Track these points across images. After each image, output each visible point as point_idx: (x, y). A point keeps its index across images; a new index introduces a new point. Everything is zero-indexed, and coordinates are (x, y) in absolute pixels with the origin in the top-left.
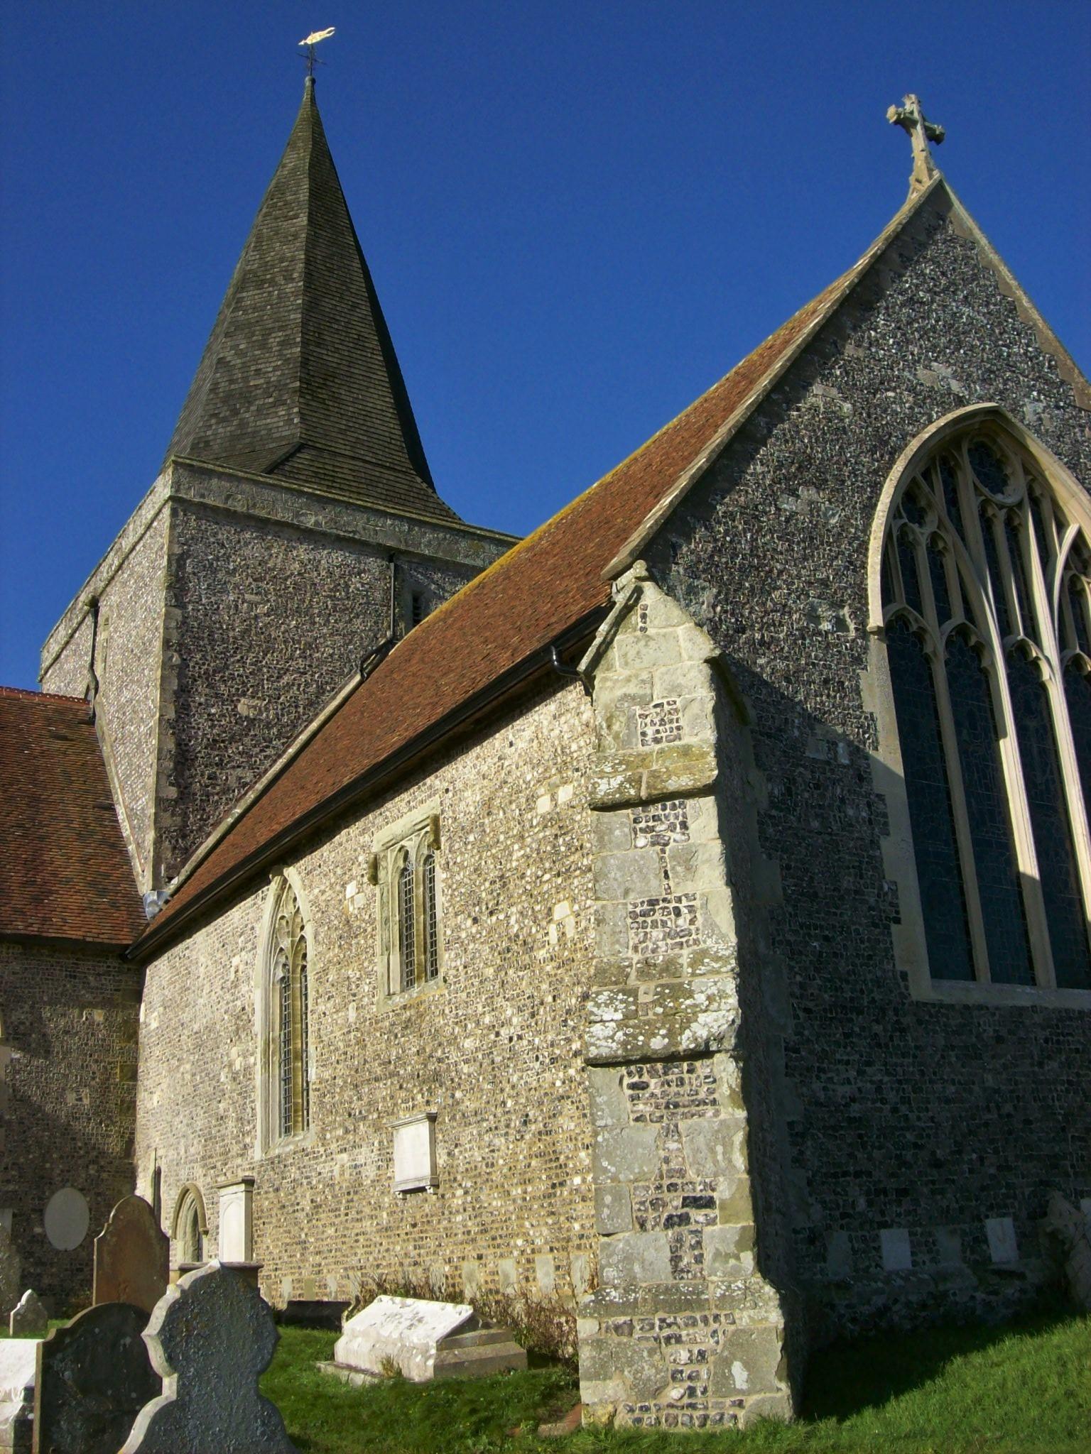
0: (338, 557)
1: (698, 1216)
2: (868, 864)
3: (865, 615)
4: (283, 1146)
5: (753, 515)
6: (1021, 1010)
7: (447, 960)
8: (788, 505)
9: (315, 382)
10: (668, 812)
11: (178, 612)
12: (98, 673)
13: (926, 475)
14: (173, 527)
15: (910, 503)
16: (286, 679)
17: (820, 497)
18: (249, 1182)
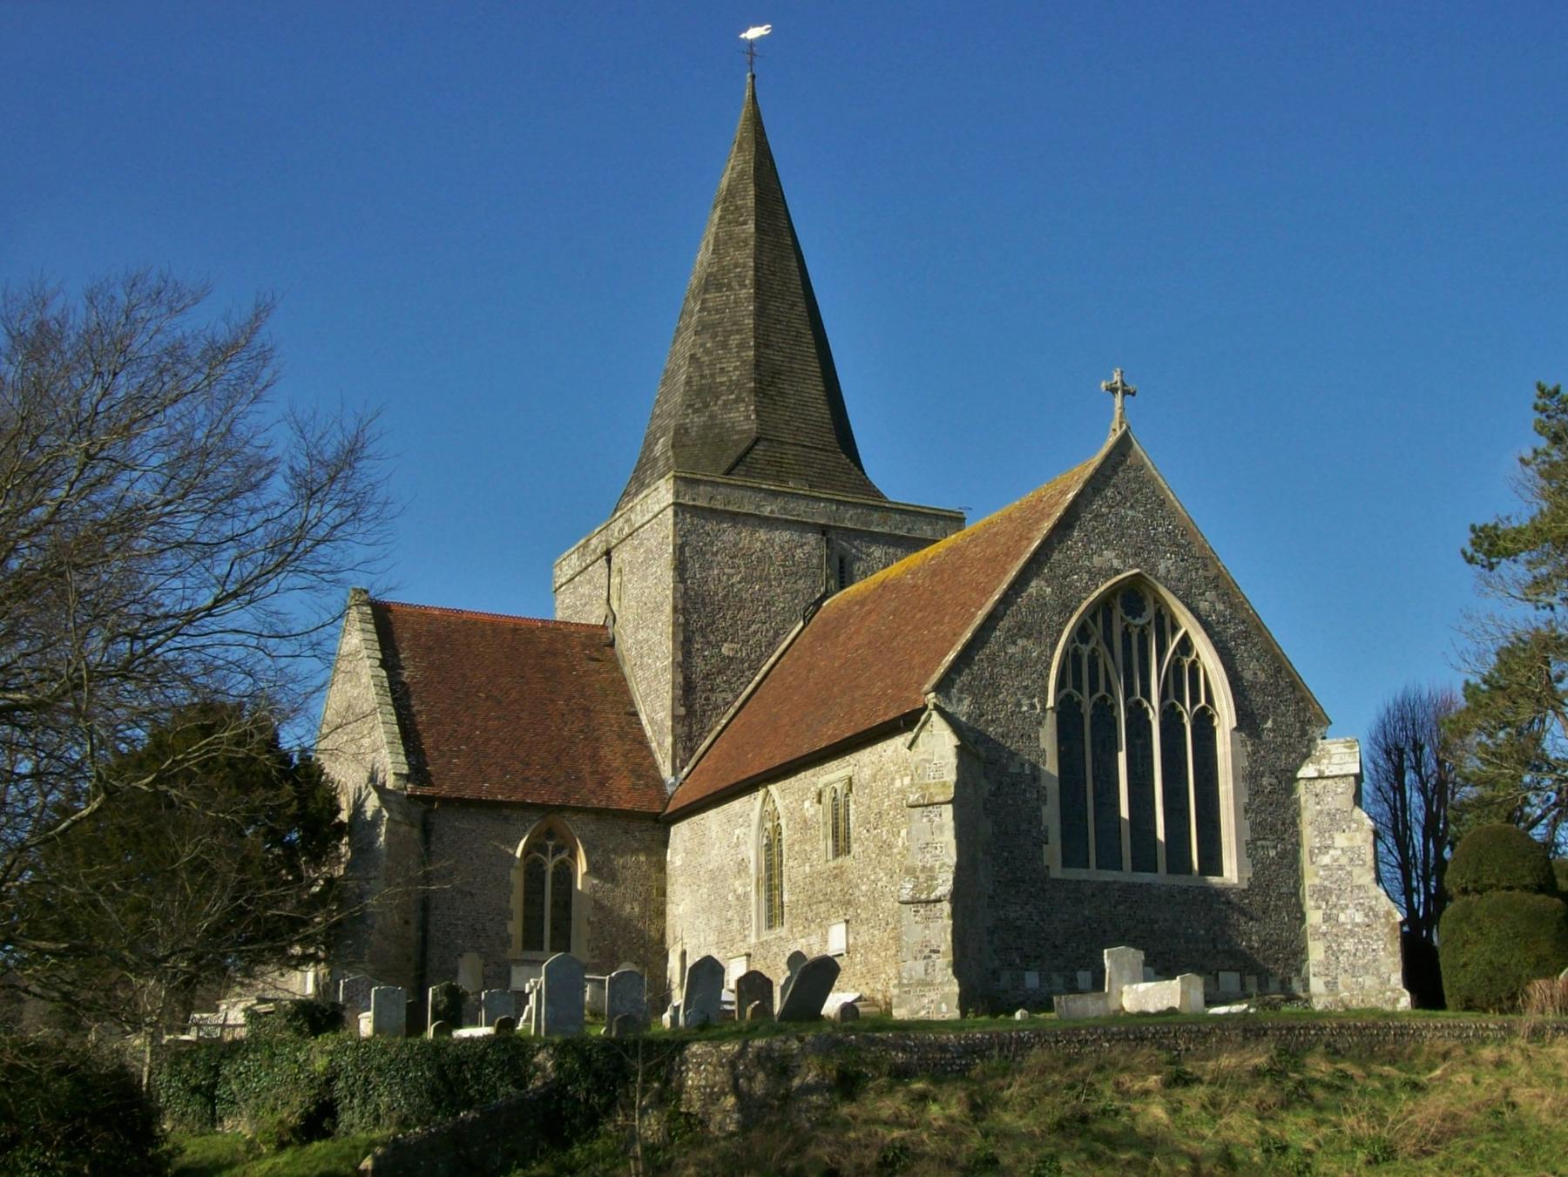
0: (786, 535)
1: (934, 956)
2: (1035, 817)
3: (1046, 700)
4: (767, 936)
5: (992, 659)
6: (1107, 883)
7: (855, 848)
8: (1011, 650)
9: (767, 381)
10: (935, 810)
11: (681, 586)
12: (615, 607)
13: (1093, 617)
14: (675, 524)
15: (1082, 633)
16: (754, 627)
17: (1029, 644)
18: (748, 955)
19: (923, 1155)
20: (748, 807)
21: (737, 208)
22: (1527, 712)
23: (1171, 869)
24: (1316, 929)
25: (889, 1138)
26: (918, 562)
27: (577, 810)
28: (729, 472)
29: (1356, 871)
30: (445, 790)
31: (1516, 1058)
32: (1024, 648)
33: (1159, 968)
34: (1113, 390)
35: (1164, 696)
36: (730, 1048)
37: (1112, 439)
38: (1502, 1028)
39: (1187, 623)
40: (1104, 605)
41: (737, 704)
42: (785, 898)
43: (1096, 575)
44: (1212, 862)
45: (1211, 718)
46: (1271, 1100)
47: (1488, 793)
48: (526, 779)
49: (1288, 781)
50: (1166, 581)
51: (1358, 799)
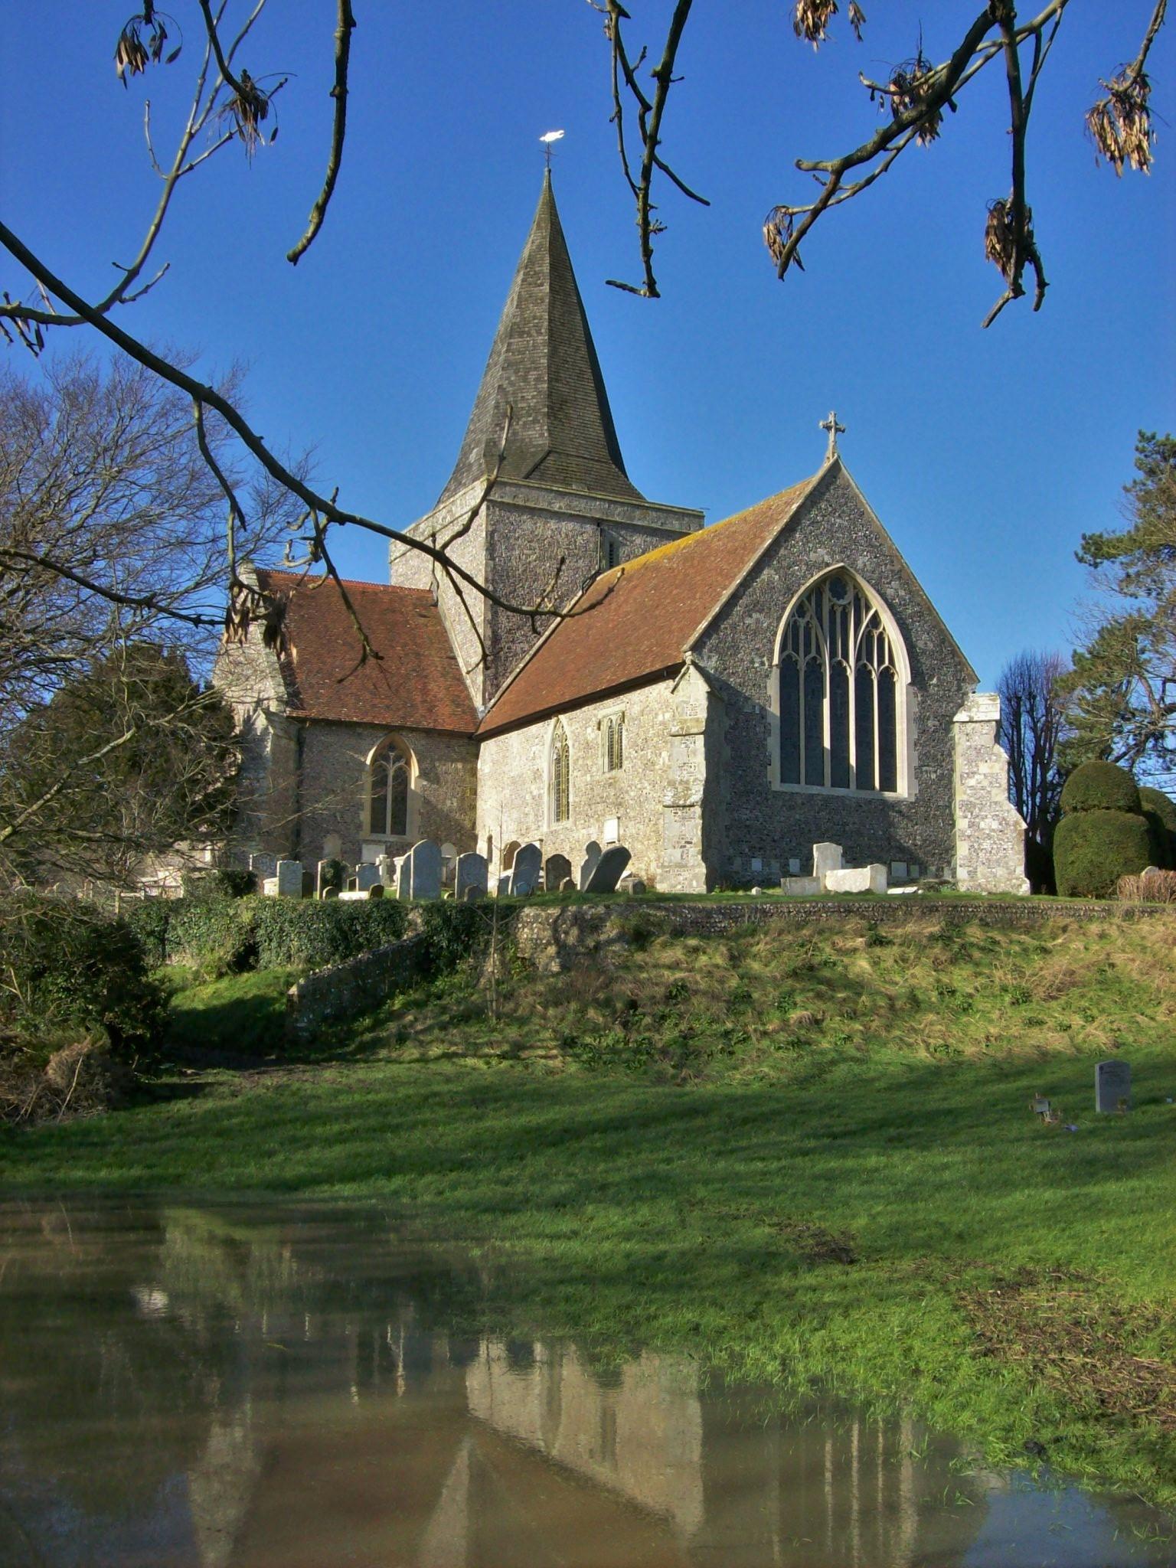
0: (571, 525)
2: (762, 745)
4: (555, 826)
5: (734, 627)
7: (626, 764)
8: (748, 621)
9: (557, 407)
13: (809, 598)
15: (800, 610)
17: (761, 617)
19: (696, 992)
20: (542, 731)
21: (536, 273)
22: (1118, 674)
23: (859, 787)
24: (963, 832)
25: (672, 979)
26: (673, 550)
27: (412, 730)
28: (527, 477)
29: (994, 791)
30: (313, 714)
31: (1114, 932)
32: (758, 621)
33: (853, 860)
34: (828, 428)
35: (858, 659)
36: (554, 911)
37: (826, 465)
38: (1104, 910)
39: (877, 604)
40: (817, 590)
41: (532, 652)
42: (571, 800)
43: (812, 567)
44: (889, 782)
45: (893, 675)
46: (943, 958)
47: (1087, 735)
48: (374, 706)
49: (947, 723)
50: (862, 572)
51: (997, 739)
